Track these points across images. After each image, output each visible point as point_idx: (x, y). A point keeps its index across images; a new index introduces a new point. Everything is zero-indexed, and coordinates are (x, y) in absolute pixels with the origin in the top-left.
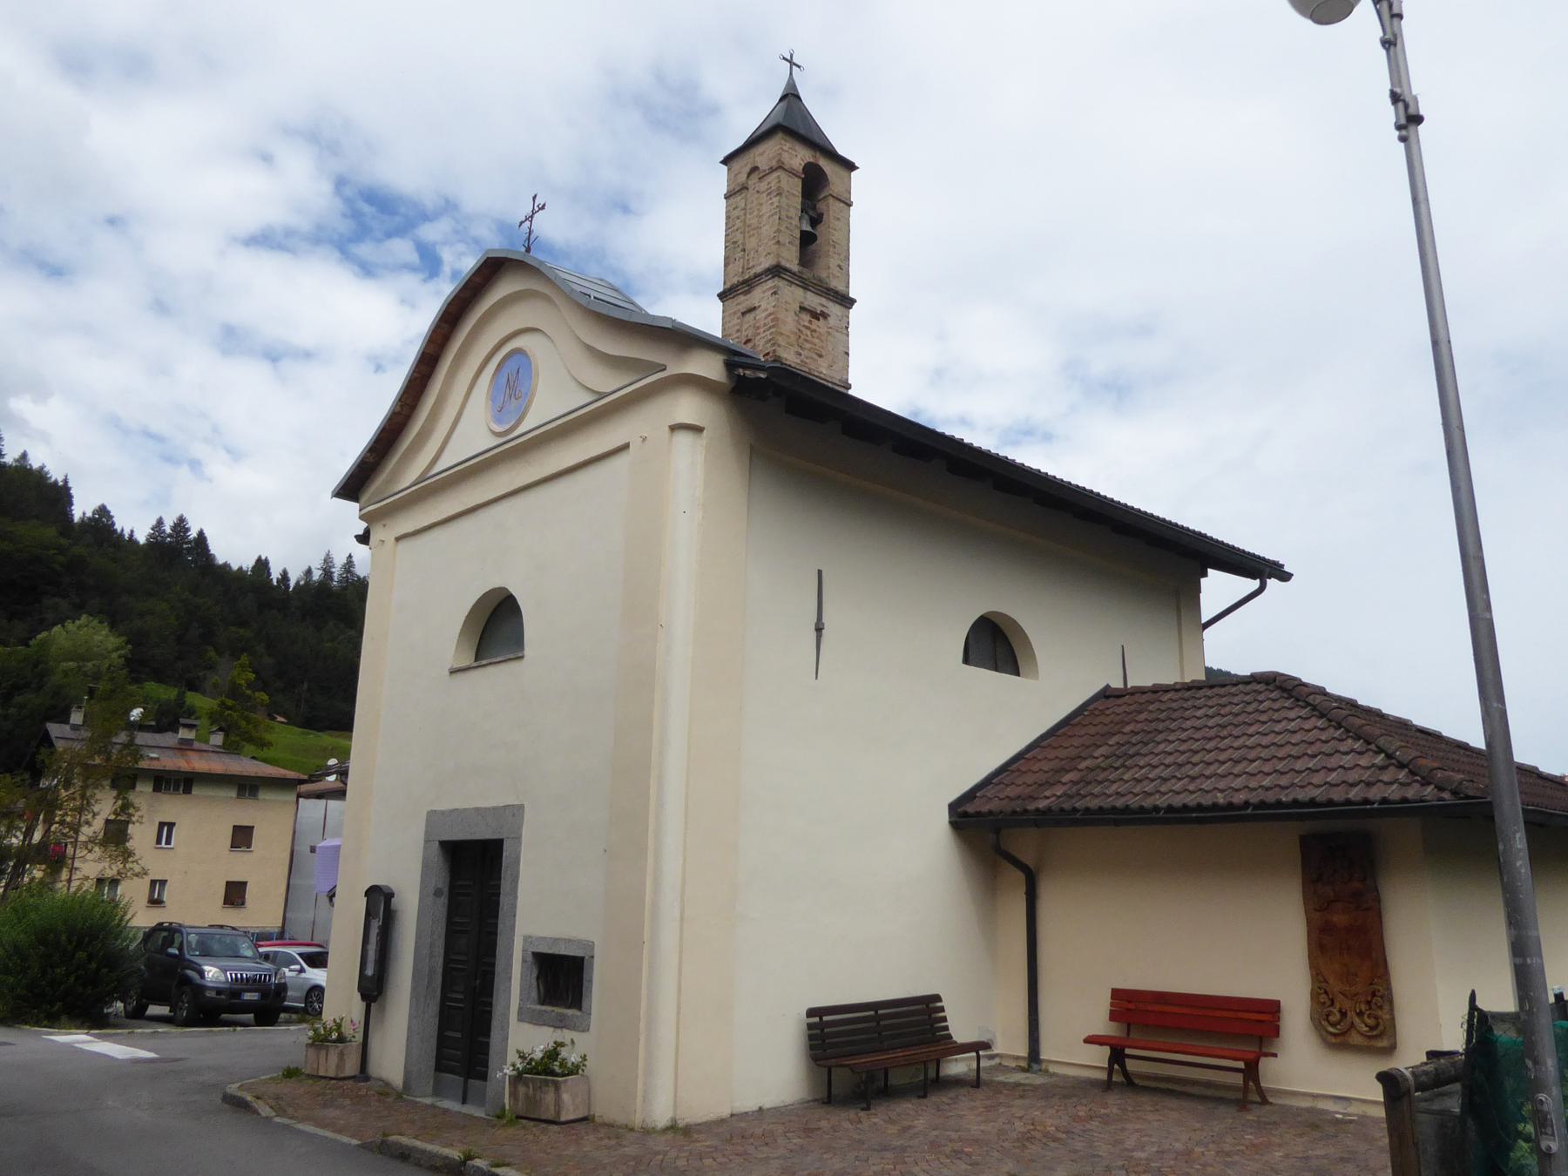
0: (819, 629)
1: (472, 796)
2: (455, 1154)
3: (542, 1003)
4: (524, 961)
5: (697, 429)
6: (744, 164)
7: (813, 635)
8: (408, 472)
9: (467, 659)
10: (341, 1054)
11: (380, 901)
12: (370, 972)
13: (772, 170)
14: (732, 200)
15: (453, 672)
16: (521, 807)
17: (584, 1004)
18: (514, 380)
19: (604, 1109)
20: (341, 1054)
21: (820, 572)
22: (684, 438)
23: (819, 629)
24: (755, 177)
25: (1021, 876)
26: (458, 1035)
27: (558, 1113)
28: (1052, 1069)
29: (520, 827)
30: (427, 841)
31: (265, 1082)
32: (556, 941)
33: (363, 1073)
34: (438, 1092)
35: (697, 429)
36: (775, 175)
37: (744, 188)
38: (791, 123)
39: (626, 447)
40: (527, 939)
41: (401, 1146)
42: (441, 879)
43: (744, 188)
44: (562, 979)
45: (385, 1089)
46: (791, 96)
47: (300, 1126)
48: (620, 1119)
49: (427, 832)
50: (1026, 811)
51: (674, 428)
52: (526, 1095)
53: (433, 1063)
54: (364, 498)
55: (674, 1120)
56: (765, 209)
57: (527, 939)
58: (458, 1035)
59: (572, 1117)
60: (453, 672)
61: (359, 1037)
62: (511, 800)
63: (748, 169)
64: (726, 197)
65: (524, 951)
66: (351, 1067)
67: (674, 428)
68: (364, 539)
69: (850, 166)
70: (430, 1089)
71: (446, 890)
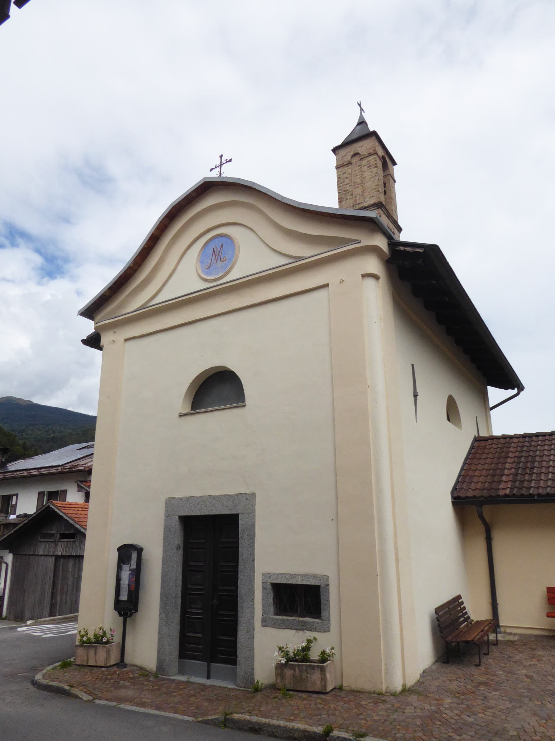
0: (416, 396)
1: (208, 487)
2: (319, 730)
3: (276, 614)
4: (264, 588)
5: (376, 277)
6: (348, 152)
7: (413, 398)
8: (134, 301)
9: (188, 410)
10: (108, 652)
11: (128, 553)
12: (124, 597)
13: (370, 155)
14: (341, 169)
15: (182, 415)
16: (253, 495)
17: (324, 614)
18: (219, 250)
19: (349, 683)
20: (108, 652)
21: (413, 365)
22: (371, 282)
23: (416, 396)
24: (356, 159)
25: (482, 528)
26: (200, 635)
27: (325, 687)
28: (508, 630)
29: (253, 505)
30: (168, 516)
31: (174, 692)
32: (294, 576)
33: (121, 663)
34: (181, 672)
35: (376, 277)
36: (372, 157)
37: (350, 163)
38: (363, 135)
39: (326, 286)
40: (264, 575)
41: (250, 722)
42: (178, 539)
43: (350, 163)
44: (300, 600)
45: (143, 672)
46: (362, 123)
47: (122, 706)
48: (368, 687)
49: (166, 511)
50: (498, 495)
51: (364, 276)
52: (294, 676)
53: (177, 653)
54: (98, 318)
55: (404, 686)
56: (366, 174)
57: (264, 575)
58: (200, 635)
59: (331, 689)
60: (182, 415)
61: (117, 639)
62: (243, 490)
63: (352, 154)
64: (337, 168)
65: (263, 582)
66: (114, 659)
67: (364, 276)
68: (93, 341)
69: (394, 163)
70: (176, 669)
71: (182, 545)
